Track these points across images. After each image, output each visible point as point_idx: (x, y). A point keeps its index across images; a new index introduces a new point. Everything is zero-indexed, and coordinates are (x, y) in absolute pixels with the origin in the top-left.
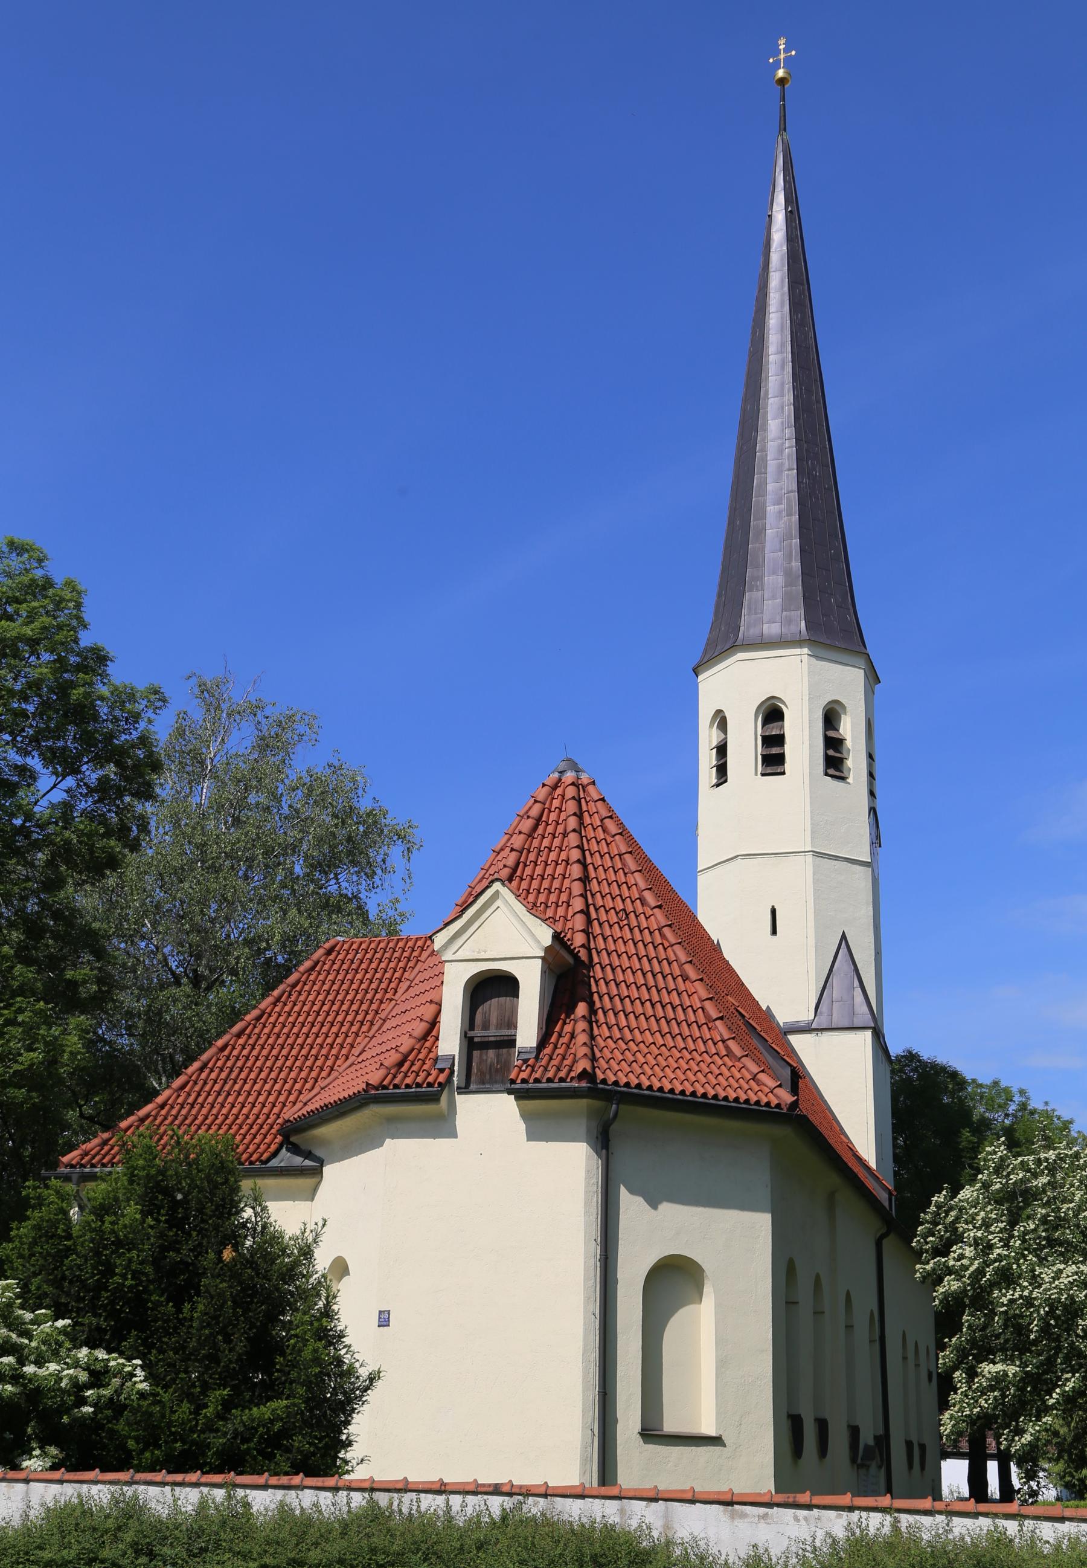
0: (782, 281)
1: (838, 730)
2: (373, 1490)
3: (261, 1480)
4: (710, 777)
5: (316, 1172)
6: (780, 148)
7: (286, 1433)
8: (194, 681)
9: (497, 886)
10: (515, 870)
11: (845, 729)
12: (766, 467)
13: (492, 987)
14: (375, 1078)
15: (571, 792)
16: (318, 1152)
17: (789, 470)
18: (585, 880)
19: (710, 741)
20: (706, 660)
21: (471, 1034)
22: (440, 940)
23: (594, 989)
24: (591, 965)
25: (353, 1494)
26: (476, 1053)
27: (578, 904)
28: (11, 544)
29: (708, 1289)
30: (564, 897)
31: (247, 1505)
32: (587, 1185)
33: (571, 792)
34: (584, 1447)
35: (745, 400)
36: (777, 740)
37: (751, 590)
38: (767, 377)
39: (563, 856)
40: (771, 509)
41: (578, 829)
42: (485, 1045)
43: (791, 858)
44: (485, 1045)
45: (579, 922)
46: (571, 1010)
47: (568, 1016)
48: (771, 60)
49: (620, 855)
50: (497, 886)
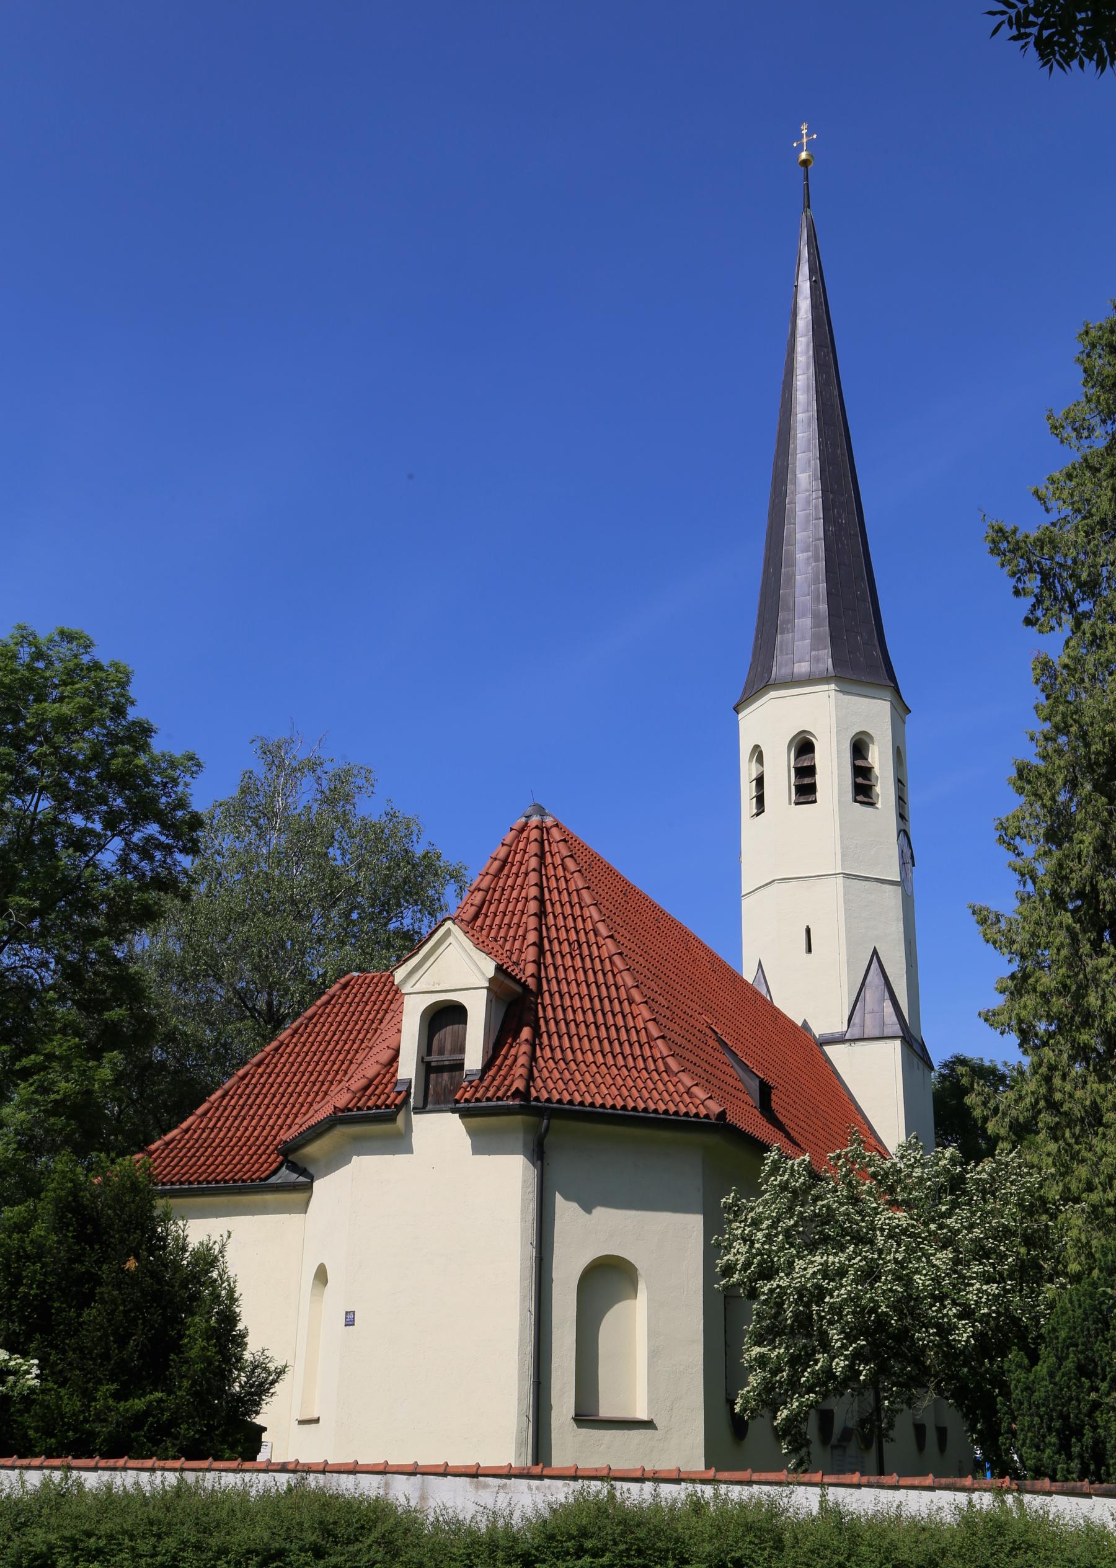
0: (808, 345)
1: (866, 759)
3: (91, 1463)
4: (751, 808)
5: (308, 1187)
6: (804, 224)
7: (173, 1422)
8: (259, 743)
11: (873, 758)
13: (445, 1016)
15: (535, 834)
16: (311, 1170)
17: (816, 519)
18: (541, 914)
19: (750, 775)
21: (427, 1059)
23: (541, 1014)
24: (540, 992)
25: (166, 1473)
26: (433, 1076)
27: (532, 937)
28: (62, 633)
29: (642, 1287)
30: (521, 932)
31: (80, 1485)
32: (524, 1193)
33: (535, 834)
34: (519, 1432)
36: (811, 771)
37: (782, 633)
39: (523, 894)
40: (800, 556)
41: (537, 868)
42: (440, 1069)
43: (824, 880)
44: (440, 1069)
45: (531, 954)
46: (516, 1035)
47: (514, 1040)
49: (578, 891)
50: (449, 924)
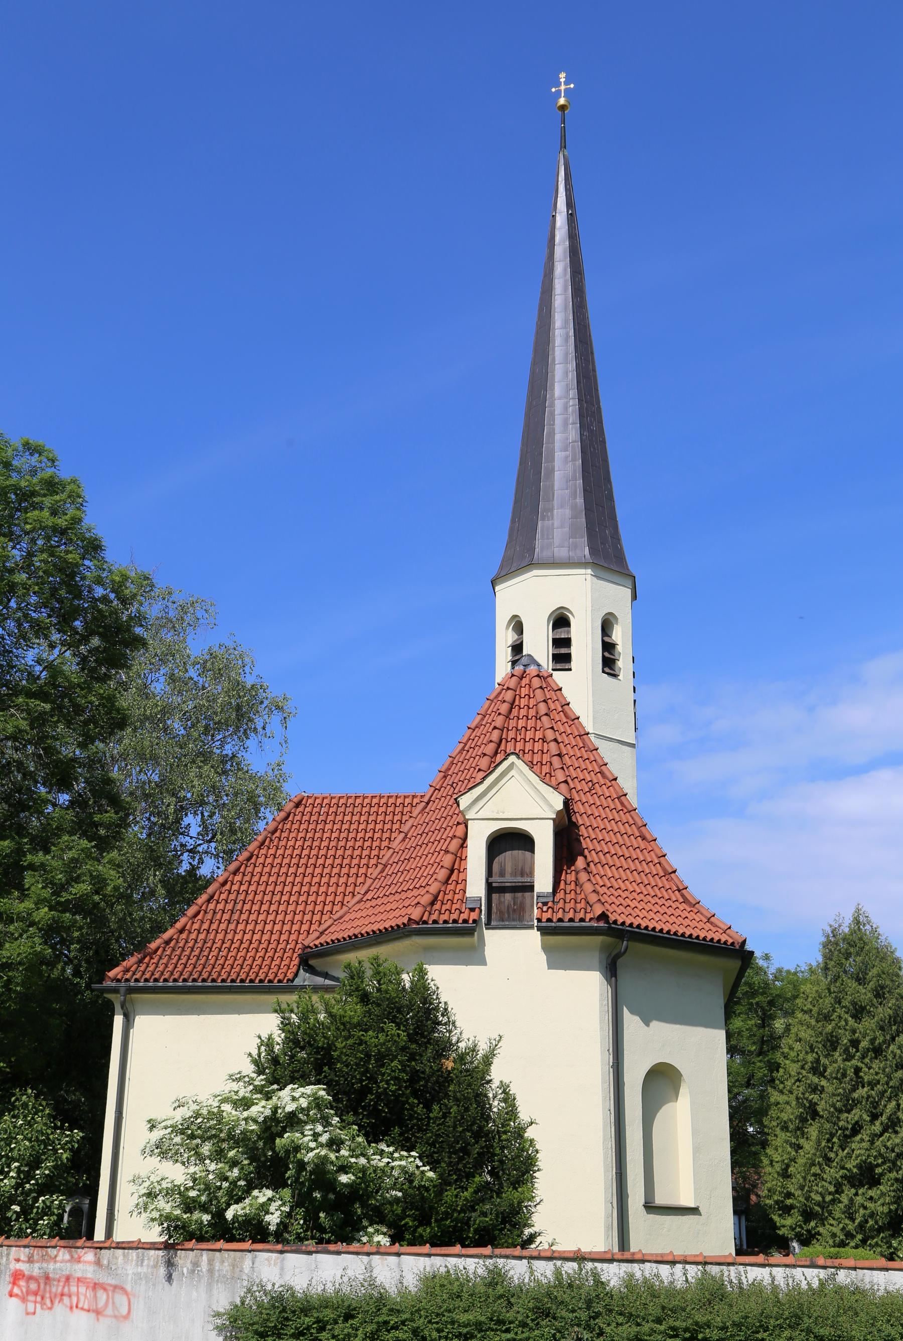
0: (565, 270)
1: (610, 637)
2: (706, 1263)
9: (512, 758)
10: (499, 745)
11: (616, 636)
12: (554, 420)
13: (509, 841)
14: (416, 914)
19: (506, 640)
20: (503, 573)
21: (491, 880)
22: (464, 801)
25: (688, 1267)
26: (495, 896)
29: (684, 1090)
35: (534, 363)
36: (566, 642)
37: (543, 519)
38: (554, 347)
42: (502, 890)
44: (502, 890)
48: (553, 90)
50: (512, 758)
